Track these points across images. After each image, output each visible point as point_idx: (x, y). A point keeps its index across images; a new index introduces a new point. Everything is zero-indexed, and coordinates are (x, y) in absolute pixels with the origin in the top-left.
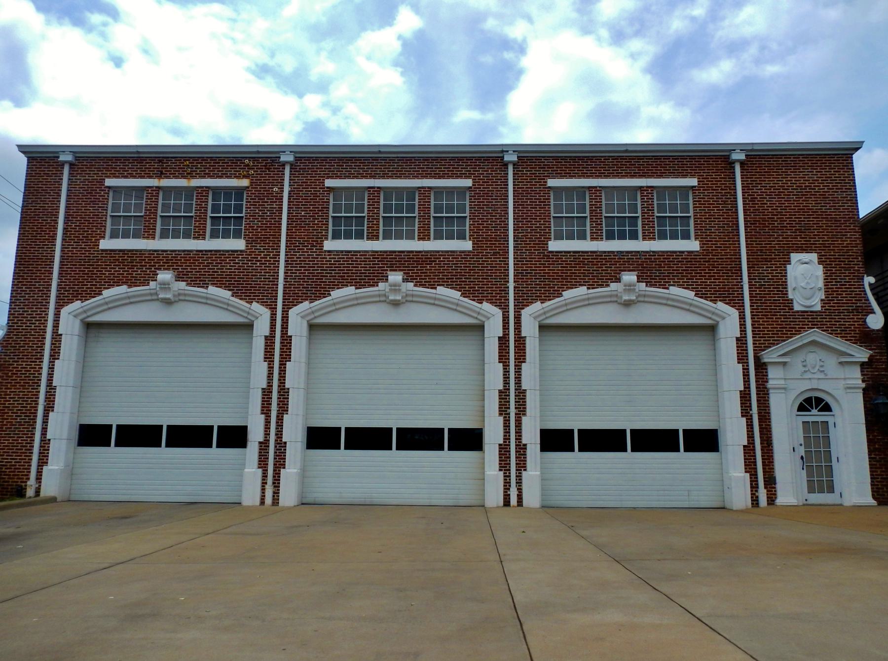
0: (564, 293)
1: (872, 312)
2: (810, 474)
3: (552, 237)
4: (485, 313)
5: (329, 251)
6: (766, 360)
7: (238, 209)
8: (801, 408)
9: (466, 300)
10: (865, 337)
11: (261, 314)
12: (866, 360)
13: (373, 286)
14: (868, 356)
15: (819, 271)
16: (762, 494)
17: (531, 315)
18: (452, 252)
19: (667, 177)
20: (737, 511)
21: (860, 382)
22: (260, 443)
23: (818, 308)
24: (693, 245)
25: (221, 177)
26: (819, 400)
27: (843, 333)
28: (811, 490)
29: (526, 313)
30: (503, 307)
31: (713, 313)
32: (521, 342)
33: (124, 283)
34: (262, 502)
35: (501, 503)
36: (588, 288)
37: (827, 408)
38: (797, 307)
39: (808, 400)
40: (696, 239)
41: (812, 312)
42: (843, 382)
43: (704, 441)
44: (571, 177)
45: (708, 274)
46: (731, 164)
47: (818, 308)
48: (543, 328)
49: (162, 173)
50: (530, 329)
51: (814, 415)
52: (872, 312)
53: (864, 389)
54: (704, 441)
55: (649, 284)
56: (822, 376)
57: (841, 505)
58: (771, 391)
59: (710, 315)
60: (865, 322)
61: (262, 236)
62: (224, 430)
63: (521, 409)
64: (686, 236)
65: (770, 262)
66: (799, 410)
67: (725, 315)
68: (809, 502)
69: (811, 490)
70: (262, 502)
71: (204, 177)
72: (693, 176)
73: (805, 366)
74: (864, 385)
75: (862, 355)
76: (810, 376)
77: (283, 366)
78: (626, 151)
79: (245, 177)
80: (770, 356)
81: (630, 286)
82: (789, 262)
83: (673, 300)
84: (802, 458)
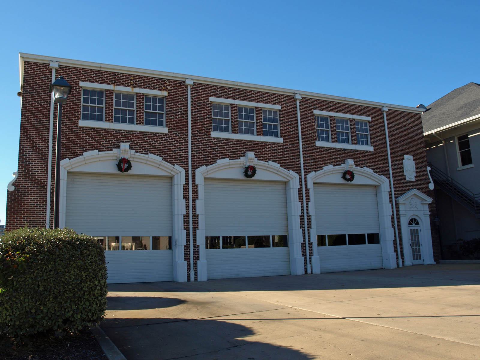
0: (217, 161)
1: (431, 183)
2: (413, 252)
3: (144, 123)
4: (291, 176)
5: (214, 138)
6: (400, 202)
7: (161, 108)
8: (410, 223)
9: (282, 168)
10: (429, 193)
11: (179, 173)
12: (431, 203)
13: (237, 158)
14: (431, 201)
15: (413, 162)
16: (400, 261)
17: (201, 172)
18: (274, 143)
19: (360, 115)
20: (393, 269)
21: (428, 212)
22: (185, 246)
23: (414, 180)
24: (371, 149)
25: (151, 88)
26: (415, 220)
27: (421, 190)
28: (414, 259)
29: (198, 171)
30: (299, 173)
31: (380, 180)
32: (195, 188)
33: (96, 148)
34: (189, 280)
35: (304, 273)
36: (230, 159)
37: (417, 223)
38: (407, 179)
39: (412, 220)
40: (281, 137)
41: (412, 181)
42: (423, 212)
43: (374, 239)
44: (323, 110)
45: (375, 162)
46: (295, 100)
47: (414, 180)
48: (206, 179)
49: (115, 82)
50: (199, 181)
51: (414, 226)
52: (431, 183)
53: (430, 215)
54: (374, 239)
55: (259, 159)
56: (416, 209)
57: (423, 264)
58: (401, 216)
59: (378, 181)
60: (428, 186)
61: (178, 125)
62: (370, 235)
63: (196, 226)
64: (161, 124)
65: (398, 157)
66: (409, 224)
67: (384, 181)
68: (414, 264)
69: (414, 259)
70: (189, 280)
71: (140, 87)
72: (369, 116)
73: (411, 205)
74: (430, 213)
75: (430, 200)
76: (413, 209)
77: (194, 201)
78: (345, 101)
79: (166, 90)
80: (401, 200)
81: (351, 166)
82: (403, 158)
83: (365, 173)
84: (411, 245)
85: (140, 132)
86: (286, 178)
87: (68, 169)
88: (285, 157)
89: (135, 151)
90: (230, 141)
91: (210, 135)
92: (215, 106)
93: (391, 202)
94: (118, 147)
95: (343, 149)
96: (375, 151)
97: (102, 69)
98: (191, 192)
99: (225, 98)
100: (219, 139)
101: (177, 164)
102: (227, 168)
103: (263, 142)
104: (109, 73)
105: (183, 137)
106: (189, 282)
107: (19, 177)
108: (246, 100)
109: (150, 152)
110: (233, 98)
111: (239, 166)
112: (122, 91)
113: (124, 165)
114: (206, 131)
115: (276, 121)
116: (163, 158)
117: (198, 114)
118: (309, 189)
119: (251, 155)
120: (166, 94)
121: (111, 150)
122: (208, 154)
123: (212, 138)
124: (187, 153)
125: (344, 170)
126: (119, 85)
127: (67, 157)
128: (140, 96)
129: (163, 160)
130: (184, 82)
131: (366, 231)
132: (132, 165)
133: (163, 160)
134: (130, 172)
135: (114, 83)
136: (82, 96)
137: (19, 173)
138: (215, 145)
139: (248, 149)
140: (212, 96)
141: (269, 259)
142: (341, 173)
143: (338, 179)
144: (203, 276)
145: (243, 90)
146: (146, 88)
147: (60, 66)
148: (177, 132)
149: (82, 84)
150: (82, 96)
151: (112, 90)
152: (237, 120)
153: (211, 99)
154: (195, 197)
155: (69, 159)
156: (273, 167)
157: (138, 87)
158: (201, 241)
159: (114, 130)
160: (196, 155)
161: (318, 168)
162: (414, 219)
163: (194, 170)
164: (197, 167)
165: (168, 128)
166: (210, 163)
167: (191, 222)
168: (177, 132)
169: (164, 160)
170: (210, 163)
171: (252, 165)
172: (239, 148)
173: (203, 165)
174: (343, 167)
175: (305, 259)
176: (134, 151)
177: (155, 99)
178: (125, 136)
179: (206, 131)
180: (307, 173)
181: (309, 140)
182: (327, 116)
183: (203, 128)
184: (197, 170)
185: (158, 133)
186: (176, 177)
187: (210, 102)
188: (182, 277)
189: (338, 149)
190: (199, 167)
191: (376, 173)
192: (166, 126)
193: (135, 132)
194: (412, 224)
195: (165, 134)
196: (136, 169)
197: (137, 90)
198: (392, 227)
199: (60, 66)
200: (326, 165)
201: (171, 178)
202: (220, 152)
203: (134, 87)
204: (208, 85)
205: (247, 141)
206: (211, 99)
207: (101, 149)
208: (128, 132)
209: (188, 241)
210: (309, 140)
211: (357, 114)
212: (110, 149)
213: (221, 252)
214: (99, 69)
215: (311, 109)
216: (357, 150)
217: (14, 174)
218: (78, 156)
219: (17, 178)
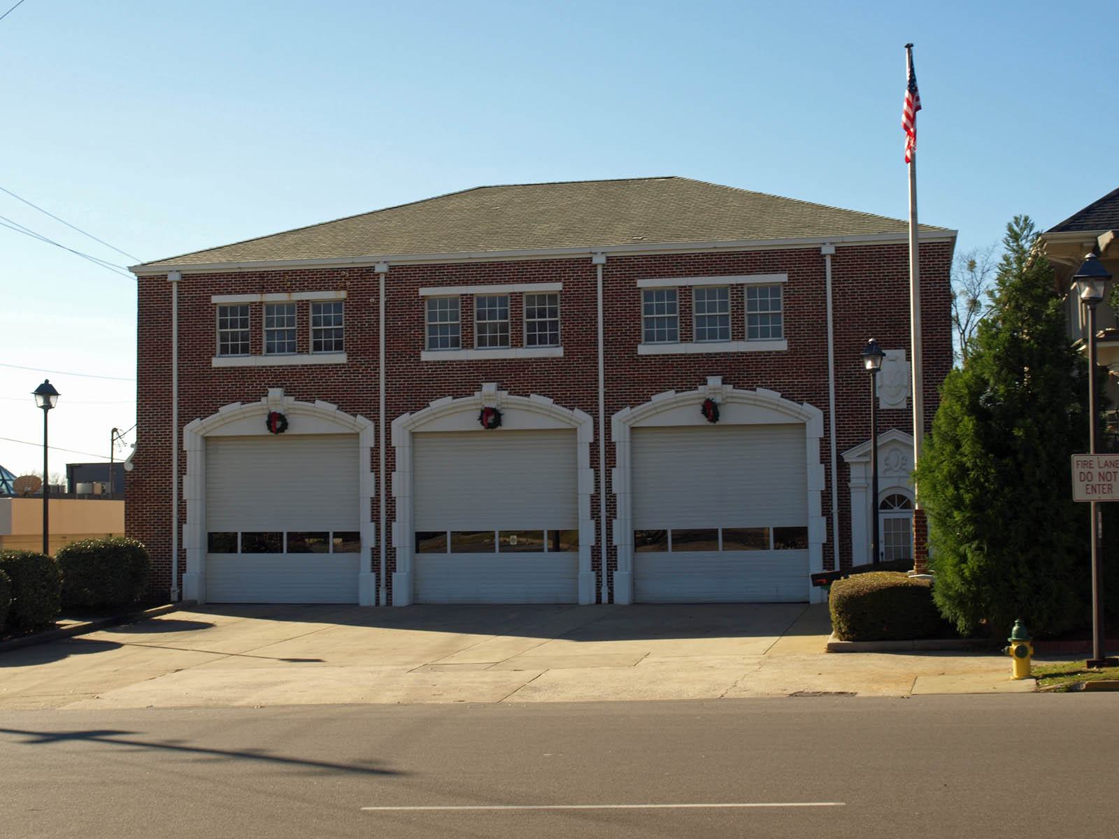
0: (653, 397)
5: (426, 362)
17: (402, 424)
18: (544, 358)
25: (319, 290)
34: (377, 603)
35: (594, 600)
43: (793, 537)
44: (661, 276)
58: (852, 490)
70: (377, 603)
71: (302, 290)
72: (783, 271)
73: (887, 465)
79: (344, 288)
85: (302, 366)
86: (797, 418)
87: (201, 433)
88: (566, 385)
89: (296, 398)
90: (456, 365)
91: (420, 357)
92: (432, 301)
93: (825, 459)
94: (705, 383)
95: (706, 354)
96: (793, 350)
97: (242, 271)
98: (384, 460)
99: (450, 285)
100: (435, 363)
101: (362, 414)
102: (450, 413)
103: (521, 359)
104: (253, 274)
105: (372, 366)
106: (378, 607)
107: (138, 450)
108: (491, 283)
109: (531, 392)
110: (466, 283)
111: (474, 407)
112: (536, 292)
113: (492, 418)
114: (412, 351)
115: (553, 313)
116: (339, 406)
117: (400, 323)
118: (615, 442)
119: (714, 381)
120: (343, 294)
121: (696, 388)
122: (415, 391)
123: (423, 362)
124: (387, 396)
125: (703, 398)
126: (269, 292)
127: (197, 417)
128: (303, 305)
129: (338, 409)
130: (819, 250)
131: (770, 521)
132: (289, 421)
133: (338, 409)
134: (287, 432)
135: (262, 290)
136: (218, 318)
137: (138, 444)
138: (428, 374)
139: (491, 375)
140: (423, 286)
141: (535, 574)
142: (477, 409)
143: (694, 416)
144: (401, 597)
145: (483, 265)
146: (311, 290)
147: (184, 276)
148: (363, 359)
149: (216, 299)
150: (218, 318)
151: (259, 303)
152: (685, 315)
153: (423, 292)
154: (391, 467)
155: (201, 419)
156: (663, 403)
157: (300, 290)
158: (622, 536)
159: (263, 367)
160: (393, 396)
161: (638, 399)
162: (887, 498)
163: (390, 423)
164: (615, 410)
165: (789, 340)
166: (419, 407)
167: (384, 509)
168: (363, 359)
169: (557, 404)
170: (419, 407)
171: (493, 406)
172: (474, 376)
173: (407, 411)
174: (702, 392)
175: (599, 576)
176: (293, 398)
177: (327, 305)
178: (279, 377)
179: (412, 351)
180: (611, 410)
181: (623, 342)
182: (673, 287)
183: (405, 345)
184: (394, 421)
185: (331, 365)
186: (361, 434)
187: (422, 296)
188: (366, 596)
189: (693, 354)
190: (398, 416)
191: (346, 412)
192: (785, 337)
193: (294, 367)
194: (892, 508)
195: (343, 364)
196: (509, 422)
197: (298, 296)
198: (593, 518)
199: (184, 276)
200: (660, 392)
201: (574, 431)
202: (436, 386)
203: (293, 291)
204: (418, 267)
205: (489, 360)
206: (423, 292)
207: (245, 400)
208: (284, 368)
209: (598, 540)
210: (623, 342)
211: (749, 273)
212: (257, 399)
213: (241, 560)
214: (238, 271)
215: (632, 280)
216: (742, 353)
217: (132, 446)
218: (212, 414)
219: (136, 452)
